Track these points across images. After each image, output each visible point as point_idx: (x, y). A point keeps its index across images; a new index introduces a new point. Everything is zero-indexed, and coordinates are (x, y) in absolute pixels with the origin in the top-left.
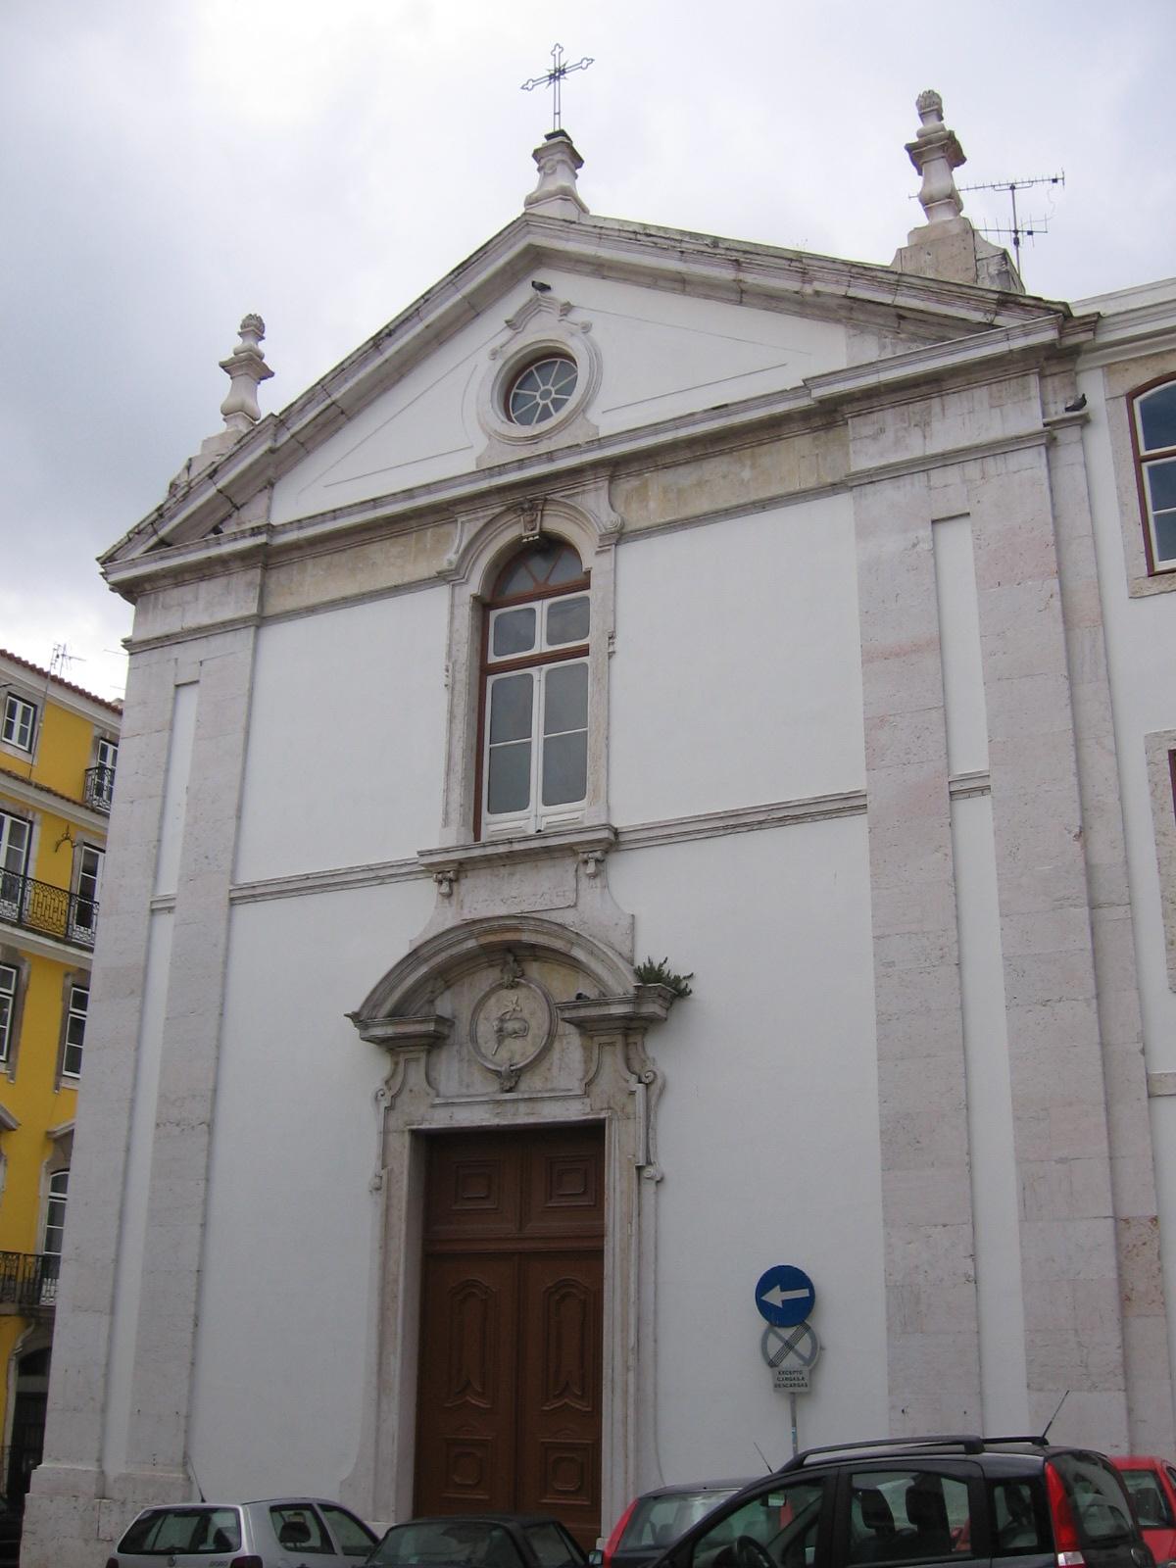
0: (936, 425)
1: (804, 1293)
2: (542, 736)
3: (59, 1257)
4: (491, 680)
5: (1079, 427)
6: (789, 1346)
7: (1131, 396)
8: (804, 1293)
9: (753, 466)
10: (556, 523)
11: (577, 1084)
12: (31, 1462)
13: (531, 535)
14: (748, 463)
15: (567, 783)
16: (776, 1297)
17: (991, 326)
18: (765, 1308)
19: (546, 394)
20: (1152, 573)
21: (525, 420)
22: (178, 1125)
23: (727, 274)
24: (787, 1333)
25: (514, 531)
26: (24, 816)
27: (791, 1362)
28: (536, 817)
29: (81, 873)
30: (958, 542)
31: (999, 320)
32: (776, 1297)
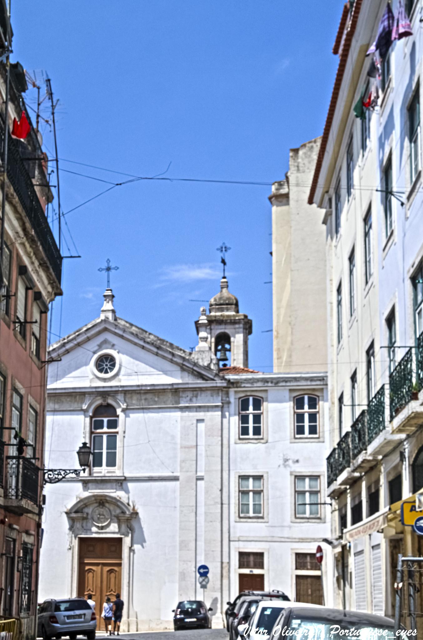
0: (199, 398)
1: (206, 570)
2: (117, 451)
3: (262, 577)
4: (93, 435)
5: (216, 391)
6: (204, 580)
7: (239, 398)
8: (206, 570)
9: (158, 397)
10: (110, 401)
11: (238, 535)
12: (178, 623)
13: (105, 404)
14: (157, 396)
15: (112, 462)
16: (202, 571)
17: (213, 380)
18: (200, 573)
19: (107, 365)
20: (240, 439)
21: (101, 371)
22: (382, 532)
23: (160, 352)
24: (203, 578)
25: (99, 401)
26: (316, 502)
27: (204, 583)
28: (102, 471)
29: (365, 520)
30: (201, 426)
31: (216, 379)
32: (202, 571)
